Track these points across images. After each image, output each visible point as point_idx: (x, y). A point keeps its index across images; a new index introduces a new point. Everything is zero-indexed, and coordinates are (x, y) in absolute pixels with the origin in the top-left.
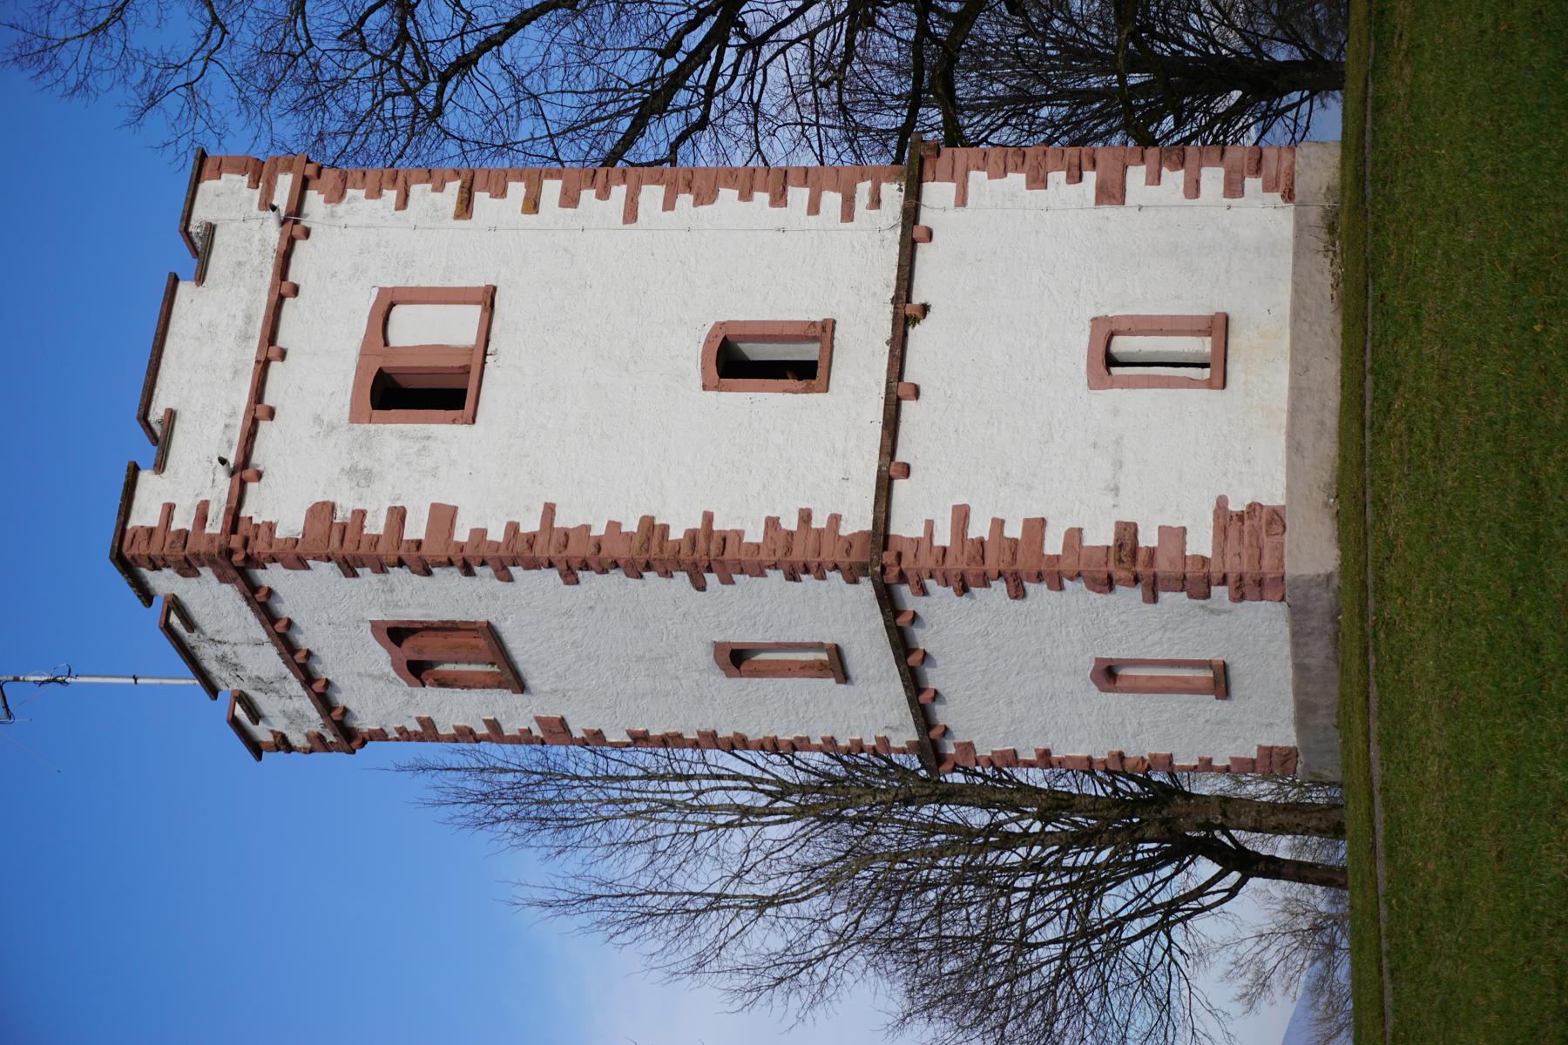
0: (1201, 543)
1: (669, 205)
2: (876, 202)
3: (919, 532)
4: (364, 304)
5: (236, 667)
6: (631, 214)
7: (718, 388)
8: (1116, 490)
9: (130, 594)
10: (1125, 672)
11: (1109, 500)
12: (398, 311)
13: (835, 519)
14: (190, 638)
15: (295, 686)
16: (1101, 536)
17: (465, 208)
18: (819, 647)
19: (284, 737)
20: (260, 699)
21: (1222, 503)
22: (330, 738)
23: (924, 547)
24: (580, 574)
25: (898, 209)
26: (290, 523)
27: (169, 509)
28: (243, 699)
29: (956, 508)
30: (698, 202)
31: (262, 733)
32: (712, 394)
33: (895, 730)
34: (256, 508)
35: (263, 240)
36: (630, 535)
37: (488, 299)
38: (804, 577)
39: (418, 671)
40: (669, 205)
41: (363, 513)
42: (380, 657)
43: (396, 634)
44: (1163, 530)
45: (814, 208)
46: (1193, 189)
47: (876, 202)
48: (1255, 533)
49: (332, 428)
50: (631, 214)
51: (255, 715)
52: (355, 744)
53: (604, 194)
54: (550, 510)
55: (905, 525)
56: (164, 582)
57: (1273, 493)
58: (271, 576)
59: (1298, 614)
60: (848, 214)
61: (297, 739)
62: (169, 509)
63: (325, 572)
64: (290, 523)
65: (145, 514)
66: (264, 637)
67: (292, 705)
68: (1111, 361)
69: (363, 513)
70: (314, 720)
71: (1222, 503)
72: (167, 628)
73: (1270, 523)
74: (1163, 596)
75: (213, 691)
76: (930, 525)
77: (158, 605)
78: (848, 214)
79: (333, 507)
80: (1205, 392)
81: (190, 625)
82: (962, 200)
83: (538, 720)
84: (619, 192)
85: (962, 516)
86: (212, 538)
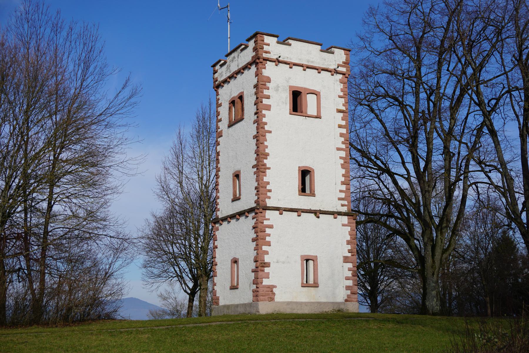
1: (341, 158)
2: (343, 205)
3: (267, 217)
5: (233, 61)
7: (299, 170)
8: (278, 262)
9: (249, 36)
11: (275, 261)
13: (269, 198)
14: (239, 50)
15: (229, 74)
16: (267, 259)
17: (339, 111)
20: (225, 66)
21: (275, 287)
22: (217, 83)
23: (264, 218)
25: (341, 211)
27: (268, 45)
28: (225, 63)
30: (342, 165)
31: (217, 67)
34: (269, 65)
35: (331, 65)
37: (318, 117)
38: (256, 191)
39: (233, 103)
40: (341, 158)
42: (235, 94)
43: (241, 98)
45: (341, 191)
47: (343, 205)
48: (268, 294)
49: (288, 82)
50: (338, 149)
51: (222, 66)
53: (343, 143)
54: (270, 132)
56: (252, 44)
57: (277, 299)
58: (253, 68)
60: (340, 199)
61: (216, 75)
62: (268, 45)
63: (255, 81)
66: (240, 67)
68: (307, 260)
70: (220, 79)
71: (275, 287)
74: (253, 273)
75: (227, 56)
76: (269, 219)
77: (246, 43)
78: (340, 199)
79: (270, 82)
82: (344, 225)
83: (222, 130)
84: (343, 146)
86: (262, 55)
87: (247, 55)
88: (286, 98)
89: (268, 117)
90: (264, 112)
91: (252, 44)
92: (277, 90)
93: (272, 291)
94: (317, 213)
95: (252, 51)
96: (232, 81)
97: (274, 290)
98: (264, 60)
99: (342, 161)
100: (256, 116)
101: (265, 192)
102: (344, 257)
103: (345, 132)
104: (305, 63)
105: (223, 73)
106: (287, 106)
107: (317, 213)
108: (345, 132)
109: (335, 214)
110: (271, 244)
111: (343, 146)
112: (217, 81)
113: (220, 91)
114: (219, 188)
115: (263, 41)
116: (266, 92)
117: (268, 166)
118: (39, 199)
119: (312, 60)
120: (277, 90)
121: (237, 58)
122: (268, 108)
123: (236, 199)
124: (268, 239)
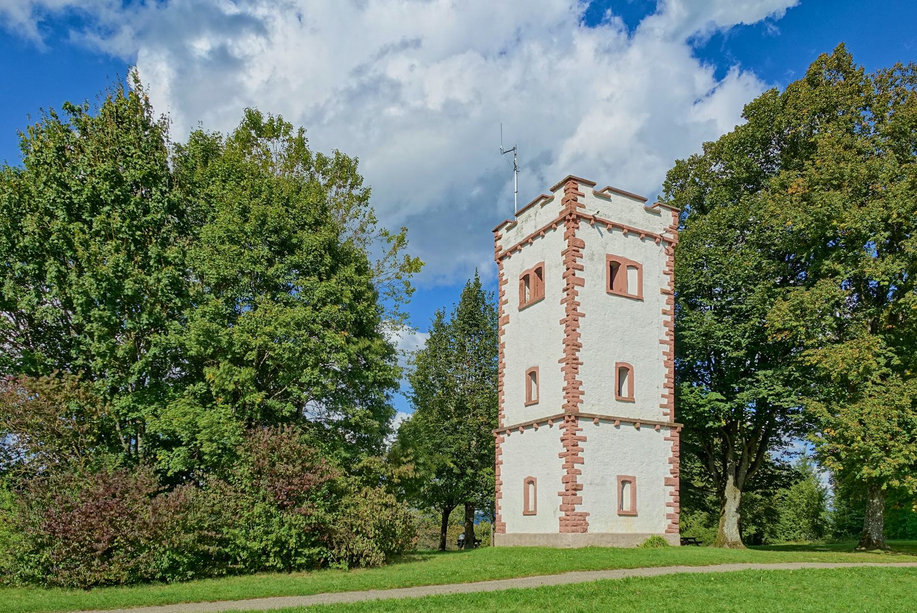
0: (579, 509)
1: (664, 353)
2: (665, 414)
3: (579, 427)
4: (638, 259)
5: (526, 221)
6: (662, 342)
7: (616, 367)
8: (591, 484)
9: (556, 183)
10: (531, 486)
11: (589, 482)
12: (636, 271)
13: (582, 402)
14: (538, 205)
15: (520, 240)
16: (579, 480)
17: (665, 293)
18: (538, 397)
19: (500, 238)
20: (515, 229)
21: (587, 514)
22: (500, 253)
23: (576, 428)
24: (564, 325)
25: (663, 421)
26: (579, 234)
27: (583, 196)
28: (515, 224)
29: (586, 438)
30: (665, 362)
31: (503, 231)
32: (614, 365)
33: (507, 420)
34: (582, 224)
35: (655, 229)
36: (577, 340)
37: (639, 299)
38: (565, 392)
39: (526, 278)
40: (664, 353)
41: (581, 257)
42: (531, 265)
43: (539, 271)
44: (581, 498)
45: (663, 396)
46: (668, 505)
47: (665, 414)
48: (581, 525)
49: (605, 248)
50: (662, 342)
51: (508, 229)
52: (498, 261)
53: (667, 334)
54: (584, 316)
55: (581, 424)
56: (560, 194)
57: (592, 529)
58: (562, 228)
59: (555, 536)
60: (662, 406)
61: (499, 243)
62: (583, 196)
63: (564, 245)
64: (579, 234)
65: (582, 188)
66: (538, 228)
67: (512, 239)
68: (624, 483)
69: (581, 257)
70: (506, 248)
71: (587, 514)
72: (543, 197)
73: (583, 529)
74: (561, 498)
75: (517, 215)
76: (581, 430)
77: (550, 194)
78: (662, 406)
79: (583, 248)
80: (617, 507)
81: (542, 205)
82: (666, 439)
83: (508, 315)
84: (667, 338)
85: (584, 440)
86: (575, 209)
87: (555, 209)
88: (603, 269)
89: (583, 294)
90: (576, 288)
91: (560, 194)
92: (592, 259)
93: (585, 520)
94: (638, 424)
95: (560, 203)
96: (515, 255)
97: (587, 518)
98: (578, 216)
99: (666, 358)
100: (566, 293)
101: (577, 395)
102: (666, 478)
103: (670, 320)
104: (625, 224)
105: (508, 239)
106: (604, 282)
107: (638, 424)
108: (670, 320)
109: (656, 426)
110: (585, 461)
111: (667, 338)
112: (501, 250)
113: (505, 262)
114: (504, 390)
115: (577, 189)
116: (579, 261)
117: (580, 361)
118: (123, 408)
119: (634, 220)
120: (592, 259)
121: (534, 216)
122: (581, 283)
123: (530, 403)
124: (580, 454)
